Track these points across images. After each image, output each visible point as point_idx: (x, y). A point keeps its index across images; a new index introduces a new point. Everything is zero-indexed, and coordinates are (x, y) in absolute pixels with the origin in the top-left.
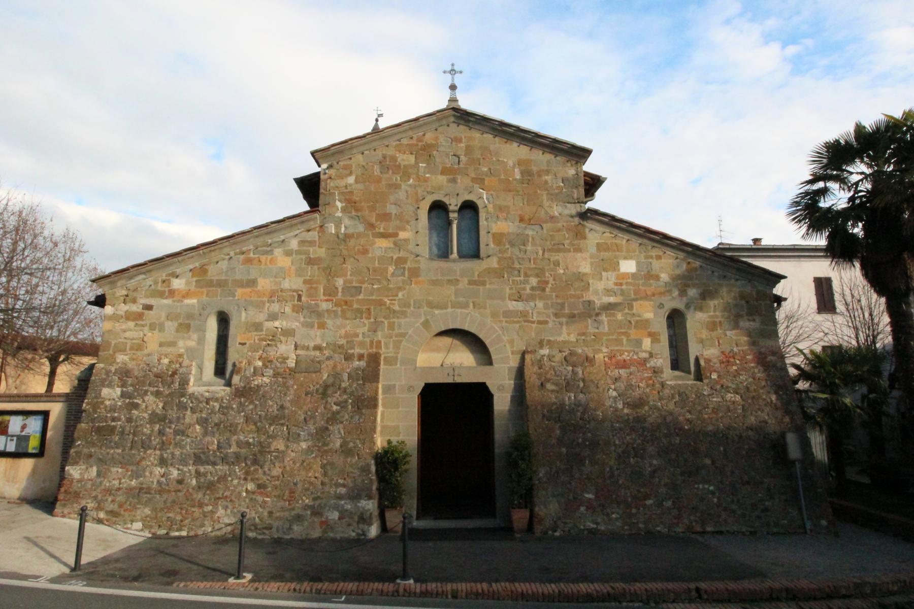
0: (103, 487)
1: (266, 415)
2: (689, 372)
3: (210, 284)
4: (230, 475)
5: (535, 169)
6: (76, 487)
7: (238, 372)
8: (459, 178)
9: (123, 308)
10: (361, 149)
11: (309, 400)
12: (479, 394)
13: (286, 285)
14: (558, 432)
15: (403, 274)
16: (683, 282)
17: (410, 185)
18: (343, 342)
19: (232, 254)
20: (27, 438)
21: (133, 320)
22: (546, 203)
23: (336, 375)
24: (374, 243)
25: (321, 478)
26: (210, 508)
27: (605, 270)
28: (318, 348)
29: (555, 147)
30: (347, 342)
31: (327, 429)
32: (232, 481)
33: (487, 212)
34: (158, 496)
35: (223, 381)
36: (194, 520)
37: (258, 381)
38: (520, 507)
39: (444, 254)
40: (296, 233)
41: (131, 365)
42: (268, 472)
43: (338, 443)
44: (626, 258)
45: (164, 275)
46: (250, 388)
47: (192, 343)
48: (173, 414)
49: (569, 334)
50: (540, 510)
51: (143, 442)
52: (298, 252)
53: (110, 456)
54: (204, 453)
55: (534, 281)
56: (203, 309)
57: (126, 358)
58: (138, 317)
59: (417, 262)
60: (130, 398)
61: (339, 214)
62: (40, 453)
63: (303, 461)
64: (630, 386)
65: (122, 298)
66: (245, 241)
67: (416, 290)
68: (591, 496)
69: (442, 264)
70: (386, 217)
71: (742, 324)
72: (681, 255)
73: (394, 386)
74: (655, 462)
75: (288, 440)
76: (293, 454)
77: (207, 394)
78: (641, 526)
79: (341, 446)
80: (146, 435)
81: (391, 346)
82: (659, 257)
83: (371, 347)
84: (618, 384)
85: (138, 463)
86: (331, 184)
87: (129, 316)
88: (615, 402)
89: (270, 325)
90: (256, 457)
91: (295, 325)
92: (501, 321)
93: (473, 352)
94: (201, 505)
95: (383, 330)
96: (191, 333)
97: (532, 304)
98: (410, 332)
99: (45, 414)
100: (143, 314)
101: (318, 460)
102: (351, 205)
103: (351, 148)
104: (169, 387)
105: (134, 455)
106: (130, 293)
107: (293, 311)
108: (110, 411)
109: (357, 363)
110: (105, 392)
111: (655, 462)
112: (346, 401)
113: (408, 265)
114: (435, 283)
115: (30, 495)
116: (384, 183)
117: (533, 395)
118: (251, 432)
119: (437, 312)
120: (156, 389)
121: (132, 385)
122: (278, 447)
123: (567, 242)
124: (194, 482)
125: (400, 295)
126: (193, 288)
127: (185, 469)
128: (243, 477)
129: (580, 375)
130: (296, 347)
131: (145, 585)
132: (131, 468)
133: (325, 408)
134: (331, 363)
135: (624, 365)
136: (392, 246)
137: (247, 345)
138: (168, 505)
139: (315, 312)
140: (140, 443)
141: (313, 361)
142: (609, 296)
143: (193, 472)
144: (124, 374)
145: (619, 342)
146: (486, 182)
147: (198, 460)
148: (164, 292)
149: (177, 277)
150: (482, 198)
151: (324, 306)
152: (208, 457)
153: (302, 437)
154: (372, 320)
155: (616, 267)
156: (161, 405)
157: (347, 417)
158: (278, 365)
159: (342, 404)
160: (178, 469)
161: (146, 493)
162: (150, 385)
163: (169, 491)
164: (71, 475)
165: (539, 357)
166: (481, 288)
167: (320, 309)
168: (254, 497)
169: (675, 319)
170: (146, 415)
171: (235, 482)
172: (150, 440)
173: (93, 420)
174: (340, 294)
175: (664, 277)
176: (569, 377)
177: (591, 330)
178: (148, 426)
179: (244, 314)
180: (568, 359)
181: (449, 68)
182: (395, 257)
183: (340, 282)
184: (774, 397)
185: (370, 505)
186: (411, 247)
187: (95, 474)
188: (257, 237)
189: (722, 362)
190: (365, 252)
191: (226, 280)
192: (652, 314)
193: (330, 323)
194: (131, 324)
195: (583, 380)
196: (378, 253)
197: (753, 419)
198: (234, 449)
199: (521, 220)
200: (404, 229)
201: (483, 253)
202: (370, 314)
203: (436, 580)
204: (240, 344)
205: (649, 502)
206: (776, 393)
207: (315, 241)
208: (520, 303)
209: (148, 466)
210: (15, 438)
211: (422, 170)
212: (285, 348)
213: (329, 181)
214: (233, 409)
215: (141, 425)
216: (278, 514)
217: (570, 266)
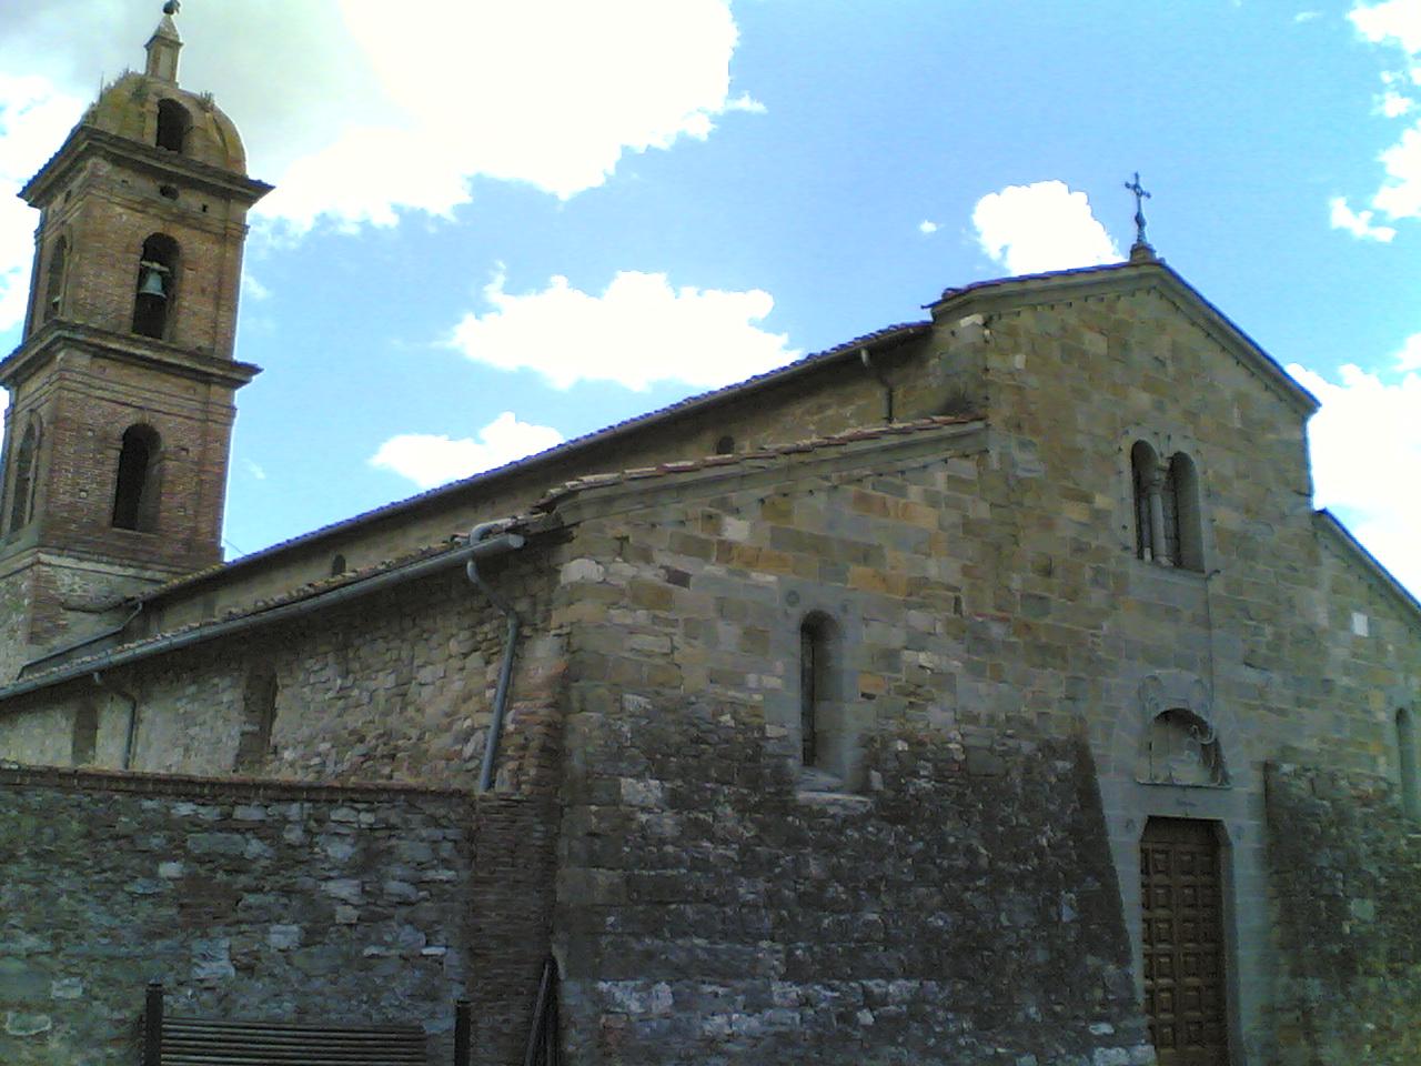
87: (637, 595)
132: (740, 985)
194: (642, 616)
212: (937, 717)
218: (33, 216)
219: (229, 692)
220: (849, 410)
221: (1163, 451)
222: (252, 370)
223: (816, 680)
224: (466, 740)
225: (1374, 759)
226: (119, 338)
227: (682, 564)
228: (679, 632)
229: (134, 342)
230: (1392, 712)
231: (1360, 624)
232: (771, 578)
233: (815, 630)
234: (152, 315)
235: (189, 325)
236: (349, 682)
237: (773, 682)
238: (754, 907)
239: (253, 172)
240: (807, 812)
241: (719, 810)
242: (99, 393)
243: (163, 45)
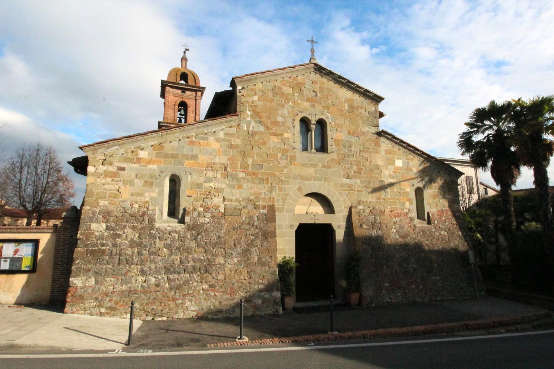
0: (101, 291)
1: (210, 241)
2: (424, 220)
3: (166, 156)
4: (191, 280)
5: (355, 105)
6: (80, 292)
7: (188, 214)
8: (316, 105)
9: (102, 168)
10: (262, 80)
11: (235, 232)
12: (328, 229)
13: (217, 160)
14: (370, 251)
15: (286, 159)
16: (423, 173)
17: (290, 106)
18: (252, 197)
19: (181, 137)
20: (20, 259)
21: (110, 177)
22: (361, 125)
23: (251, 218)
24: (269, 139)
25: (248, 280)
26: (180, 301)
27: (389, 165)
28: (237, 200)
29: (366, 94)
30: (255, 198)
31: (248, 250)
32: (193, 283)
33: (331, 126)
34: (143, 296)
35: (177, 220)
36: (170, 309)
37: (202, 220)
38: (354, 292)
39: (305, 149)
40: (223, 127)
41: (111, 208)
42: (215, 277)
43: (256, 260)
44: (398, 159)
45: (133, 147)
46: (197, 224)
47: (154, 195)
48: (146, 241)
49: (372, 198)
50: (364, 293)
51: (127, 260)
52: (224, 140)
53: (104, 270)
54: (172, 266)
55: (355, 168)
56: (162, 172)
57: (106, 203)
58: (114, 175)
59: (294, 152)
60: (113, 230)
61: (249, 119)
62: (33, 269)
63: (236, 270)
64: (401, 227)
65: (101, 161)
66: (190, 129)
67: (296, 170)
68: (387, 285)
69: (305, 154)
70: (276, 123)
71: (446, 196)
72: (422, 159)
73: (282, 224)
74: (414, 266)
75: (225, 257)
76: (230, 266)
77: (169, 228)
78: (410, 299)
79: (258, 260)
80: (128, 255)
81: (280, 201)
82: (412, 160)
83: (269, 201)
84: (396, 226)
85: (126, 274)
86: (244, 100)
87: (106, 174)
88: (395, 235)
89: (207, 185)
90: (207, 268)
91: (223, 186)
92: (339, 190)
93: (323, 206)
94: (174, 300)
95: (276, 191)
96: (154, 188)
97: (354, 181)
98: (291, 193)
99: (36, 242)
100: (118, 173)
101: (245, 269)
102: (256, 114)
103: (256, 79)
104: (141, 223)
105: (122, 269)
106: (107, 158)
107: (222, 177)
108: (99, 239)
109: (262, 211)
110: (94, 226)
111: (414, 266)
112: (258, 234)
113: (289, 154)
114: (304, 165)
115: (24, 300)
116: (275, 102)
117: (358, 232)
118: (201, 252)
119: (306, 182)
120: (132, 224)
121: (113, 221)
122: (220, 262)
123: (371, 148)
124: (167, 285)
125: (285, 171)
126: (154, 158)
127: (160, 277)
128: (199, 280)
129: (379, 221)
130: (224, 200)
131: (188, 348)
132: (120, 278)
133: (246, 237)
134: (246, 210)
135: (398, 215)
136: (280, 141)
137: (193, 197)
138: (151, 300)
139: (235, 178)
140: (125, 261)
141: (235, 208)
142: (391, 178)
143: (166, 278)
144: (106, 215)
145: (395, 203)
146: (331, 109)
147: (168, 270)
148: (133, 159)
149: (142, 149)
150: (328, 118)
151: (241, 175)
152: (175, 269)
153: (234, 255)
154: (270, 185)
155: (393, 163)
156: (137, 235)
157: (259, 243)
158: (214, 210)
159: (256, 236)
160: (155, 278)
161: (134, 294)
162: (127, 222)
163: (151, 292)
164: (75, 284)
165: (358, 210)
166: (329, 170)
167: (239, 177)
168: (208, 293)
169: (419, 192)
170: (127, 242)
171: (195, 284)
172: (133, 259)
173: (86, 245)
174: (250, 168)
175: (415, 170)
176: (373, 221)
177: (383, 196)
178: (129, 249)
179: (189, 177)
180: (372, 211)
181: (310, 39)
182: (282, 148)
183: (250, 161)
184: (460, 233)
185: (277, 294)
186: (291, 143)
188: (198, 128)
189: (438, 215)
190: (265, 143)
191: (177, 154)
192: (409, 190)
193: (245, 185)
194: (109, 180)
195: (380, 223)
196: (272, 145)
197: (453, 244)
198: (191, 263)
199: (349, 133)
200: (287, 132)
201: (329, 150)
202: (268, 181)
203: (350, 330)
204: (188, 196)
205: (413, 287)
206: (461, 231)
207: (235, 134)
208: (348, 180)
209: (133, 276)
210: (9, 260)
211: (296, 98)
212: (217, 200)
213: (242, 97)
214: (188, 238)
215: (125, 249)
216: (225, 303)
217: (373, 161)
233: (175, 181)
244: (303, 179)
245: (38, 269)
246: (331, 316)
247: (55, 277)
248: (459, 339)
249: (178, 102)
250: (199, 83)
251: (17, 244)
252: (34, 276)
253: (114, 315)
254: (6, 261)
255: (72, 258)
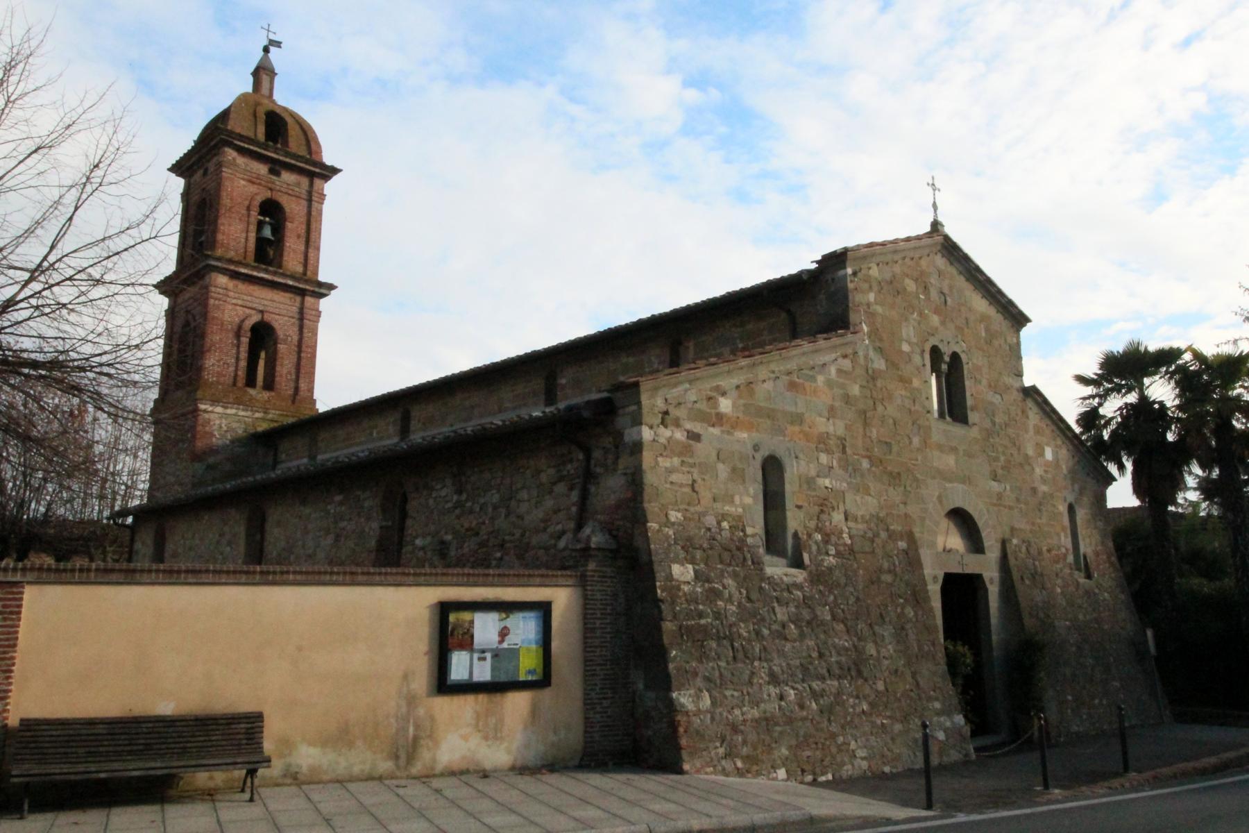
35: (784, 561)
62: (543, 681)
99: (544, 609)
106: (671, 409)
110: (676, 569)
115: (531, 758)
160: (793, 688)
164: (683, 706)
169: (1071, 509)
187: (709, 702)
199: (990, 386)
210: (488, 655)
218: (179, 183)
219: (370, 500)
220: (762, 325)
221: (947, 351)
222: (331, 287)
223: (773, 500)
224: (559, 538)
225: (1058, 535)
226: (246, 266)
227: (697, 427)
228: (695, 471)
229: (254, 268)
230: (1066, 505)
231: (1049, 454)
232: (745, 435)
233: (772, 468)
234: (267, 251)
235: (292, 262)
236: (464, 497)
237: (748, 500)
238: (749, 641)
239: (328, 159)
240: (770, 580)
241: (725, 581)
242: (234, 301)
243: (263, 73)
244: (945, 479)
245: (554, 679)
246: (1043, 757)
247: (593, 694)
248: (1045, 808)
249: (259, 199)
250: (319, 152)
251: (504, 615)
252: (546, 694)
253: (758, 774)
254: (484, 659)
255: (662, 646)
